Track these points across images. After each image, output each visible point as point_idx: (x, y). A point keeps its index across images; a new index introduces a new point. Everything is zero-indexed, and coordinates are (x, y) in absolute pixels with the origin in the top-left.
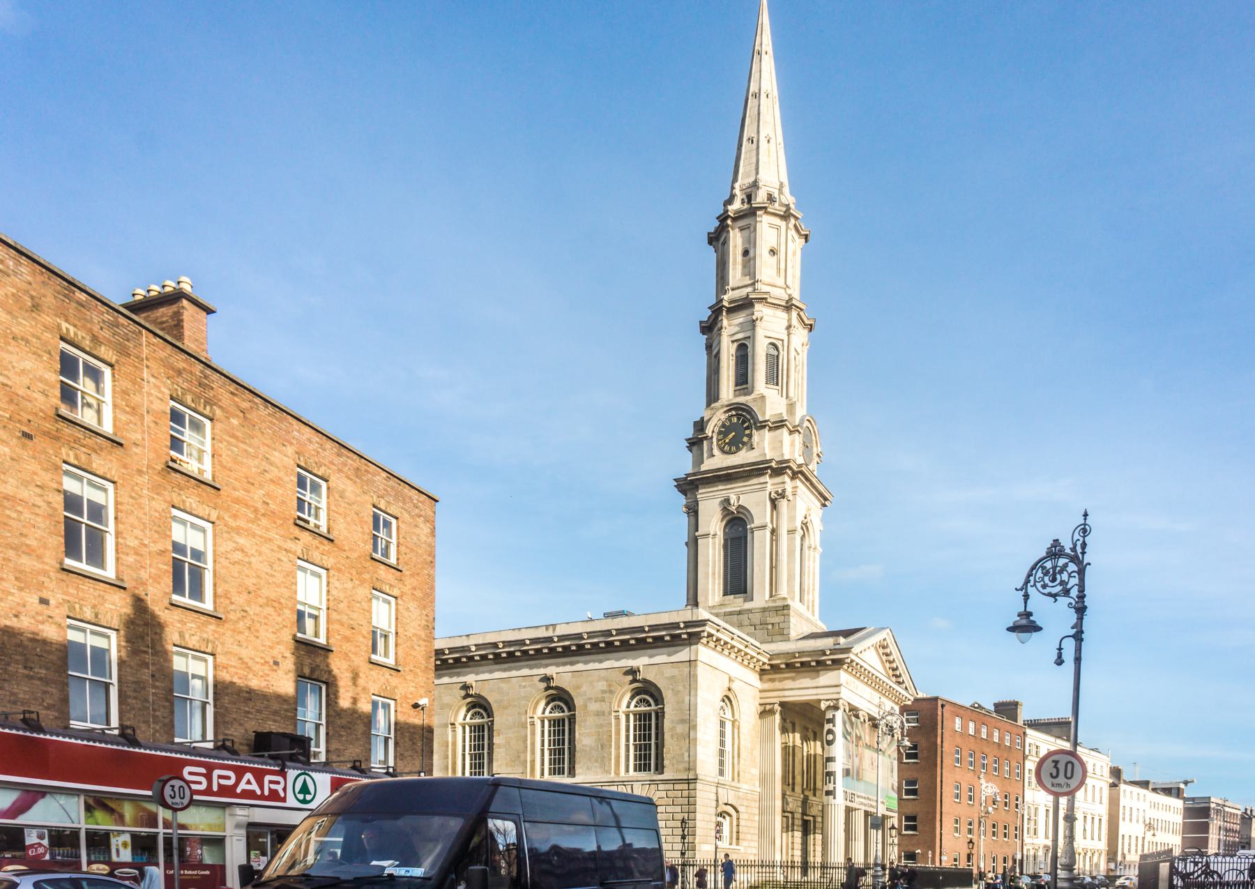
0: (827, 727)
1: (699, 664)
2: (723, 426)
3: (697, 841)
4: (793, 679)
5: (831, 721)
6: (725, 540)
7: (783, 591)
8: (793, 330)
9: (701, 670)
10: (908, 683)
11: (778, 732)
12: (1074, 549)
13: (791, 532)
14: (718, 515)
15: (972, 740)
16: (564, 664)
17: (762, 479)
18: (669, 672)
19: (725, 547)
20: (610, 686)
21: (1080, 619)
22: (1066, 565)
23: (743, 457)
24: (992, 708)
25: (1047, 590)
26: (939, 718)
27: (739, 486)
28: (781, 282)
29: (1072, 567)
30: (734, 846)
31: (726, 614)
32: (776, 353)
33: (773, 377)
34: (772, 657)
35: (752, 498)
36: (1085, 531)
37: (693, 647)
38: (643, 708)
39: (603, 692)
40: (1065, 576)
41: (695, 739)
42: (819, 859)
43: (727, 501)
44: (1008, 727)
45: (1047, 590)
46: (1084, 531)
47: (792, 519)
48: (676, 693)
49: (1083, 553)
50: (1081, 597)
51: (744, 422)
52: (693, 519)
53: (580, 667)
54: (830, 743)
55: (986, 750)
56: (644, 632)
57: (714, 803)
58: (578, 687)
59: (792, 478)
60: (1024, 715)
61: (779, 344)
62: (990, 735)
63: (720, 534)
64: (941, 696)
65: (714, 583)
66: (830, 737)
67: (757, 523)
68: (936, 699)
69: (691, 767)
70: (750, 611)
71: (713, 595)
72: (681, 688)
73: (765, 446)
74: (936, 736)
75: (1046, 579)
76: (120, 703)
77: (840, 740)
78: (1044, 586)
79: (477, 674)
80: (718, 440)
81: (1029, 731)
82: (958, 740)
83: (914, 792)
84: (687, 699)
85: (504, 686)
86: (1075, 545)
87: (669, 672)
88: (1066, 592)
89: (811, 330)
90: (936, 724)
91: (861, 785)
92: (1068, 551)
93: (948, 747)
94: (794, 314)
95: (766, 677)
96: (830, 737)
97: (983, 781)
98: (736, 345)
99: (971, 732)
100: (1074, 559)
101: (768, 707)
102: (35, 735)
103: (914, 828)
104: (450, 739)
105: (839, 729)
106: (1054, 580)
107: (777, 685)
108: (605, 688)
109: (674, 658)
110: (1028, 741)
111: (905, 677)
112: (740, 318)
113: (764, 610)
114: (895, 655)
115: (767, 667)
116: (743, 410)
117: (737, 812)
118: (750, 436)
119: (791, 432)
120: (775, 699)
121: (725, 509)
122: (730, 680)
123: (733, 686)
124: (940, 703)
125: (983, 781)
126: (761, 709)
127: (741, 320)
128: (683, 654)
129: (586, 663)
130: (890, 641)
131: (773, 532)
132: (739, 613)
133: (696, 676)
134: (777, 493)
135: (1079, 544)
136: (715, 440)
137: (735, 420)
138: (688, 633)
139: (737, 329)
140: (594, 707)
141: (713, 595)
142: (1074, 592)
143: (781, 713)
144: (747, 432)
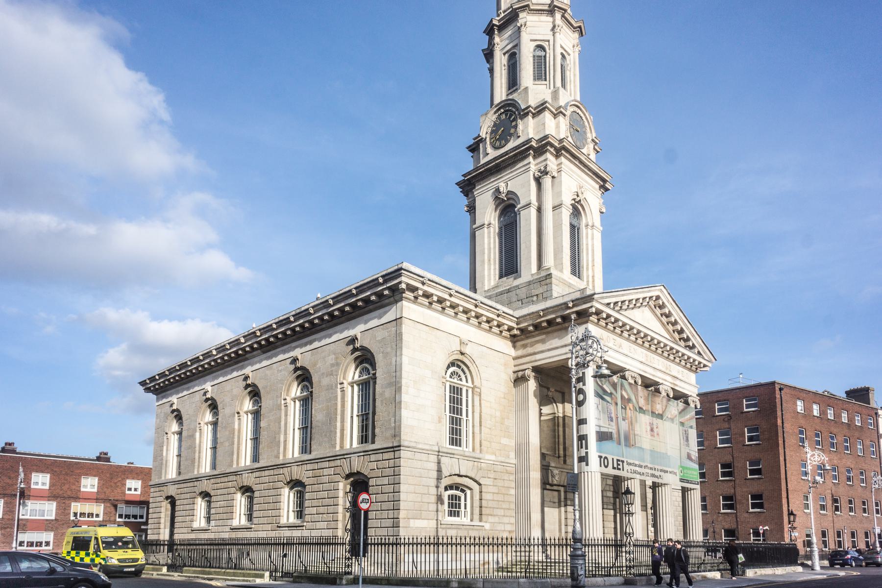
2: (495, 125)
3: (401, 516)
4: (543, 341)
5: (581, 379)
6: (500, 228)
7: (549, 261)
8: (557, 30)
9: (406, 328)
10: (700, 347)
11: (533, 402)
13: (556, 207)
14: (491, 206)
15: (818, 421)
16: (306, 345)
17: (526, 162)
18: (380, 334)
19: (500, 235)
20: (337, 358)
24: (845, 396)
26: (778, 401)
27: (507, 175)
30: (476, 522)
31: (497, 295)
33: (540, 74)
34: (519, 320)
37: (399, 304)
39: (332, 365)
41: (400, 402)
42: (49, 536)
43: (498, 190)
44: (857, 408)
47: (558, 194)
48: (386, 355)
53: (316, 344)
54: (580, 404)
55: (835, 430)
56: (353, 296)
57: (434, 474)
58: (315, 365)
59: (557, 156)
61: (545, 45)
62: (837, 416)
63: (495, 223)
64: (778, 380)
65: (489, 269)
66: (581, 397)
67: (523, 202)
68: (773, 383)
69: (397, 435)
71: (489, 280)
72: (389, 350)
73: (529, 130)
77: (592, 400)
79: (252, 365)
80: (491, 139)
82: (802, 422)
83: (758, 472)
84: (394, 360)
85: (268, 372)
87: (380, 334)
89: (581, 34)
90: (775, 406)
91: (634, 451)
93: (789, 428)
94: (558, 16)
95: (519, 344)
97: (807, 449)
98: (507, 55)
99: (816, 413)
101: (520, 374)
103: (760, 506)
104: (236, 427)
105: (590, 386)
107: (530, 350)
108: (333, 361)
109: (385, 319)
111: (695, 340)
112: (508, 32)
113: (529, 283)
114: (676, 315)
115: (515, 332)
116: (509, 105)
117: (480, 484)
118: (516, 127)
119: (555, 116)
120: (527, 365)
121: (496, 198)
122: (462, 343)
123: (467, 350)
124: (777, 387)
125: (807, 449)
126: (513, 377)
127: (510, 33)
128: (390, 315)
129: (320, 340)
130: (665, 298)
131: (539, 210)
132: (509, 291)
133: (401, 334)
134: (540, 171)
136: (488, 139)
137: (503, 117)
138: (389, 288)
139: (507, 42)
140: (325, 381)
141: (489, 280)
143: (535, 378)
144: (514, 124)
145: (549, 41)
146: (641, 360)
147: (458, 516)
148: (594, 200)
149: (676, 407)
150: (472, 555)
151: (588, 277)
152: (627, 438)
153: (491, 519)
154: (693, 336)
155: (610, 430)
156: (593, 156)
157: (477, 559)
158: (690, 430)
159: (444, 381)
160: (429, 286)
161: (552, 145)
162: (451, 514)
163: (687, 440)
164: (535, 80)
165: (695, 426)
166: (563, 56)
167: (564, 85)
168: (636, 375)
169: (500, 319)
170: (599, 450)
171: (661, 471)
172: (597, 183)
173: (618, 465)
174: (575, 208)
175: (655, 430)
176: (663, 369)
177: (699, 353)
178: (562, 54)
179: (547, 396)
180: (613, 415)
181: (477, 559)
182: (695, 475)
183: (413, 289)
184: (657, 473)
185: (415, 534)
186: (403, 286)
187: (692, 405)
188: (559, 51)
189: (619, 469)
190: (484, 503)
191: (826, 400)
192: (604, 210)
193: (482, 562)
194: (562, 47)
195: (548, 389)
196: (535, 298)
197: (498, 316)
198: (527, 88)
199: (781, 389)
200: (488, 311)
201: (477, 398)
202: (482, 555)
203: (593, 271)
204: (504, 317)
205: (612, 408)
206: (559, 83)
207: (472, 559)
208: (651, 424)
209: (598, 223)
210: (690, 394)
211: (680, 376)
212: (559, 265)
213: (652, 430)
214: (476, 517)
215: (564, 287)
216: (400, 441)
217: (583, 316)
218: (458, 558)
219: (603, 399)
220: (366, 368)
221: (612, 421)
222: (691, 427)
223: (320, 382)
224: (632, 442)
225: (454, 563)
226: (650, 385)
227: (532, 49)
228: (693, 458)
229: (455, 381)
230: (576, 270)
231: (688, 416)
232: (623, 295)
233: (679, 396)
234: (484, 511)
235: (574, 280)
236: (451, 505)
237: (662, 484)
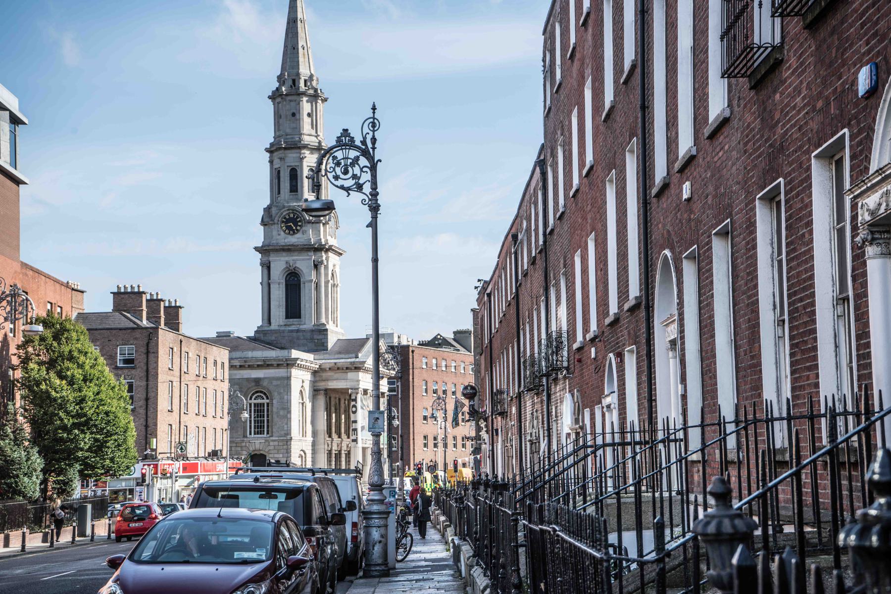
0: (353, 403)
12: (364, 142)
21: (375, 217)
22: (357, 159)
23: (293, 239)
25: (339, 183)
29: (363, 161)
35: (303, 263)
36: (374, 125)
38: (259, 401)
40: (357, 170)
45: (339, 183)
46: (374, 125)
48: (280, 393)
49: (374, 148)
50: (374, 194)
52: (266, 272)
74: (409, 375)
75: (338, 170)
76: (856, 321)
78: (336, 178)
86: (365, 138)
88: (359, 187)
92: (358, 143)
96: (354, 409)
100: (365, 153)
106: (346, 172)
113: (312, 331)
135: (369, 137)
142: (367, 188)
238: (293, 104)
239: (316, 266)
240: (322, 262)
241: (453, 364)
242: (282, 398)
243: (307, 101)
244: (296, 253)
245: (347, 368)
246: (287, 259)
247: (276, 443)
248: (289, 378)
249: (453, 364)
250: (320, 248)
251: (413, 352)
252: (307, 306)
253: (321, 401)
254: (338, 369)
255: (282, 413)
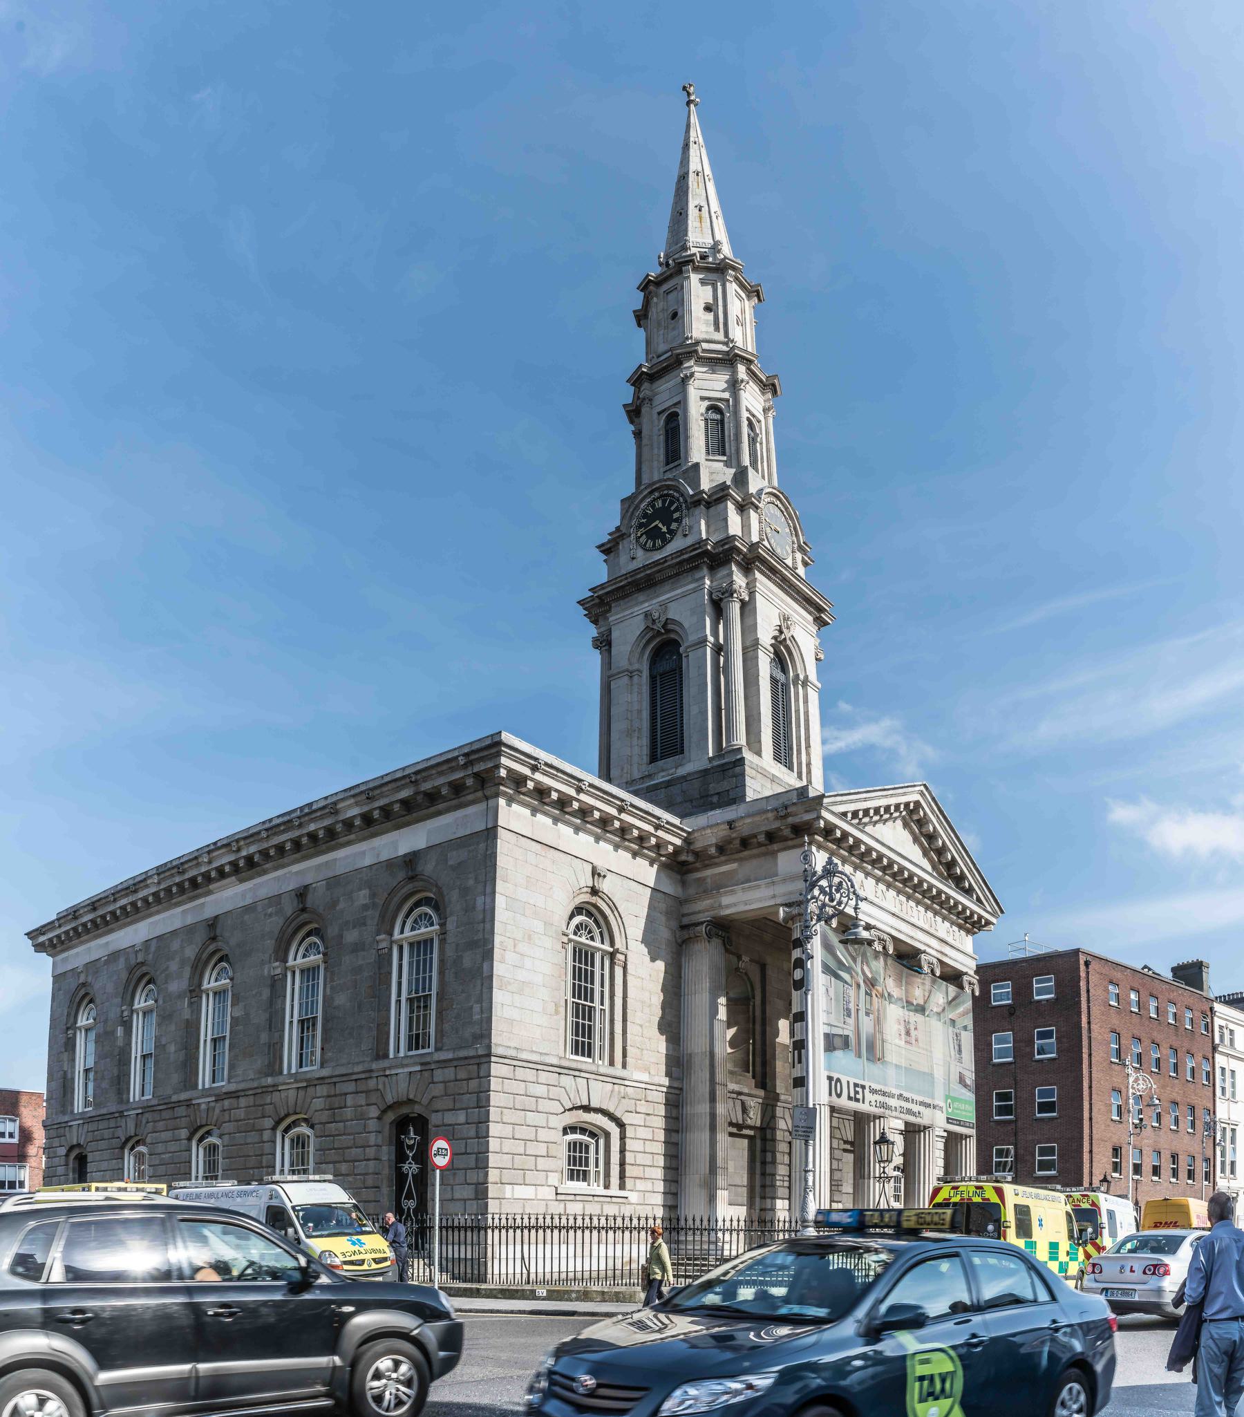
1: (500, 831)
9: (507, 851)
15: (1136, 1019)
24: (1168, 975)
28: (720, 336)
30: (614, 1190)
32: (718, 417)
44: (1190, 1001)
48: (465, 891)
51: (672, 503)
55: (1158, 1037)
58: (334, 903)
60: (1217, 983)
64: (1086, 947)
68: (1077, 952)
70: (684, 778)
74: (1080, 1013)
81: (1218, 1007)
82: (1115, 1021)
89: (775, 392)
96: (798, 974)
102: (186, 1367)
110: (1218, 1022)
113: (705, 772)
116: (669, 487)
117: (621, 1125)
122: (595, 873)
123: (605, 886)
132: (668, 784)
145: (728, 401)
146: (893, 910)
147: (584, 1180)
148: (805, 638)
149: (940, 996)
150: (610, 1247)
151: (800, 764)
152: (871, 1047)
153: (640, 1185)
154: (970, 871)
155: (846, 1033)
156: (801, 571)
157: (619, 1254)
158: (963, 1033)
159: (565, 939)
160: (545, 774)
161: (739, 551)
162: (573, 1175)
163: (960, 1051)
164: (708, 453)
165: (971, 1027)
166: (751, 425)
167: (754, 463)
168: (886, 937)
169: (660, 833)
170: (829, 1068)
171: (922, 1104)
172: (810, 613)
173: (856, 1093)
174: (777, 654)
175: (913, 1033)
176: (926, 927)
177: (979, 900)
178: (748, 419)
179: (737, 969)
180: (852, 1006)
181: (619, 1254)
182: (970, 1115)
183: (518, 781)
184: (916, 1108)
185: (517, 1209)
186: (503, 773)
187: (968, 990)
188: (745, 414)
189: (857, 1100)
190: (629, 1158)
191: (1144, 979)
192: (822, 656)
193: (626, 1259)
194: (748, 410)
195: (739, 958)
196: (715, 799)
197: (657, 827)
198: (697, 466)
199: (1087, 964)
200: (641, 819)
201: (619, 971)
202: (627, 1247)
203: (808, 754)
204: (668, 831)
205: (852, 992)
206: (746, 461)
207: (610, 1253)
208: (907, 1023)
209: (813, 677)
210: (964, 969)
211: (950, 940)
212: (754, 743)
213: (908, 1033)
214: (615, 1180)
215: (765, 777)
216: (489, 1047)
217: (802, 831)
218: (587, 1253)
219: (837, 977)
220: (426, 914)
221: (849, 1016)
222: (965, 1028)
223: (341, 936)
224: (879, 1054)
225: (579, 1260)
226: (907, 958)
227: (703, 410)
228: (968, 1082)
229: (583, 940)
230: (784, 754)
231: (961, 1009)
232: (865, 800)
233: (953, 977)
234: (630, 1171)
235: (778, 770)
236: (572, 1160)
237: (925, 1128)
238: (672, 296)
239: (718, 609)
240: (729, 592)
241: (1190, 1064)
242: (469, 908)
243: (703, 282)
244: (667, 586)
245: (771, 837)
246: (646, 606)
247: (449, 1073)
248: (490, 833)
249: (1189, 1015)
250: (722, 555)
251: (1087, 964)
252: (694, 710)
253: (705, 962)
254: (745, 843)
255: (467, 962)
